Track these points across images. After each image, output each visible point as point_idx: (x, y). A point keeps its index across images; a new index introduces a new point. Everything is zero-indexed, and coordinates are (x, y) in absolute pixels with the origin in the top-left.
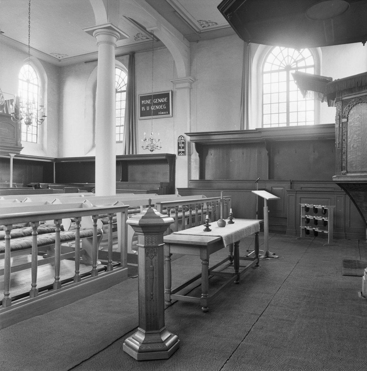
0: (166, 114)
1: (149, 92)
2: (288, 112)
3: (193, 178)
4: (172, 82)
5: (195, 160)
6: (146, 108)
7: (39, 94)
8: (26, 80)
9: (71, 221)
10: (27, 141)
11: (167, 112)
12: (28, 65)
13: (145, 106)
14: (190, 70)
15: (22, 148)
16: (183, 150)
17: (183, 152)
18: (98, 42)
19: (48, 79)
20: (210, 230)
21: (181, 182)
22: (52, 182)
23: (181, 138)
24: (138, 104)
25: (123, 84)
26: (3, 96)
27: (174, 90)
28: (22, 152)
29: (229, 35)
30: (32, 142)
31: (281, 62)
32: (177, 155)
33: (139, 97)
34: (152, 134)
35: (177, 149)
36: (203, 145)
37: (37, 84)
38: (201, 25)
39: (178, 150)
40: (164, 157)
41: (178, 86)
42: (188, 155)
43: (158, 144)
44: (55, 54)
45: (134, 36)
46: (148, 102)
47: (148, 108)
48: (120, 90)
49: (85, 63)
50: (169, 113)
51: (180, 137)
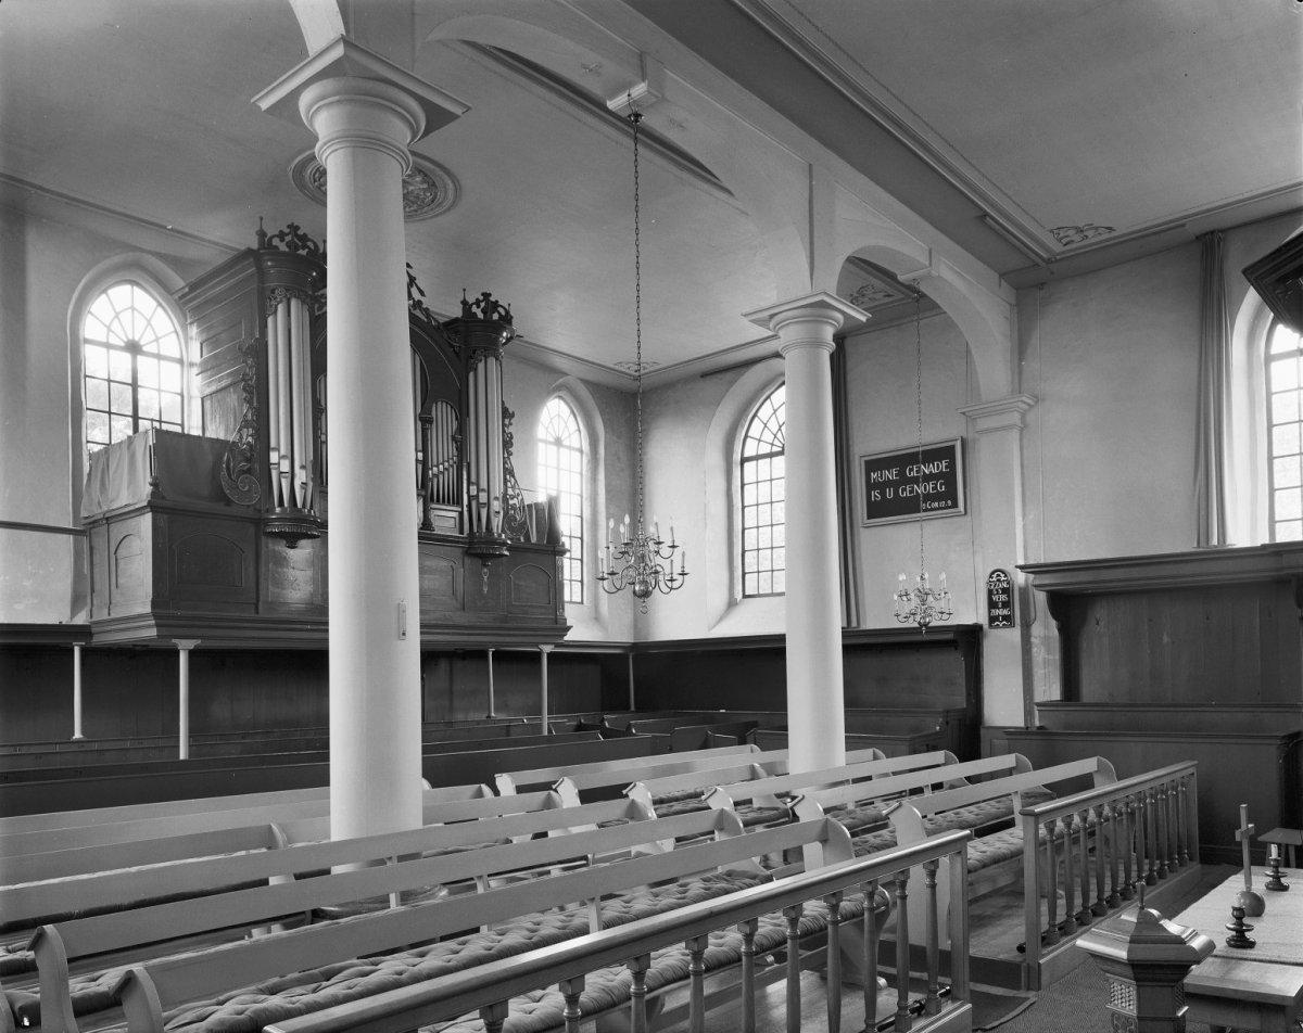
0: (947, 507)
1: (892, 448)
3: (1039, 697)
4: (964, 413)
5: (1046, 639)
6: (883, 494)
8: (123, 344)
11: (949, 502)
13: (882, 486)
14: (1020, 373)
15: (569, 628)
16: (1005, 612)
17: (1005, 618)
19: (606, 432)
20: (1251, 945)
21: (1003, 706)
23: (999, 575)
24: (858, 484)
27: (970, 436)
28: (570, 637)
32: (986, 627)
33: (863, 464)
34: (926, 576)
35: (987, 610)
36: (1073, 599)
38: (1060, 240)
39: (990, 612)
40: (950, 636)
41: (983, 424)
42: (1022, 626)
43: (942, 605)
46: (891, 475)
47: (890, 493)
49: (702, 376)
50: (955, 505)
51: (993, 573)
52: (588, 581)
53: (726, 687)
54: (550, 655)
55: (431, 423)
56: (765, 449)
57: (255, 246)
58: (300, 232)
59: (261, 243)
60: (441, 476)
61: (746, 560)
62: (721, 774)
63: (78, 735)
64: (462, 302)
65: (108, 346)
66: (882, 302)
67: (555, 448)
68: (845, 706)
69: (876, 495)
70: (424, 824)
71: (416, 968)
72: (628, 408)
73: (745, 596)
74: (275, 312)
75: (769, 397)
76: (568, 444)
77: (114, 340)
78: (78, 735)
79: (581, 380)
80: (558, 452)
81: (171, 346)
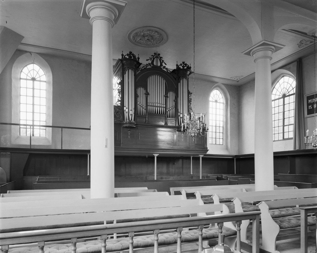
2: (283, 133)
7: (224, 109)
15: (208, 150)
18: (255, 59)
22: (232, 173)
25: (291, 88)
28: (208, 153)
29: (19, 50)
31: (27, 75)
45: (298, 44)
48: (288, 94)
52: (225, 138)
53: (239, 167)
54: (202, 158)
55: (168, 97)
56: (277, 97)
57: (121, 58)
58: (185, 63)
60: (170, 111)
63: (192, 173)
64: (122, 55)
65: (27, 79)
66: (309, 45)
67: (215, 103)
69: (310, 107)
71: (184, 236)
72: (238, 91)
74: (180, 82)
75: (278, 81)
77: (28, 78)
81: (44, 78)
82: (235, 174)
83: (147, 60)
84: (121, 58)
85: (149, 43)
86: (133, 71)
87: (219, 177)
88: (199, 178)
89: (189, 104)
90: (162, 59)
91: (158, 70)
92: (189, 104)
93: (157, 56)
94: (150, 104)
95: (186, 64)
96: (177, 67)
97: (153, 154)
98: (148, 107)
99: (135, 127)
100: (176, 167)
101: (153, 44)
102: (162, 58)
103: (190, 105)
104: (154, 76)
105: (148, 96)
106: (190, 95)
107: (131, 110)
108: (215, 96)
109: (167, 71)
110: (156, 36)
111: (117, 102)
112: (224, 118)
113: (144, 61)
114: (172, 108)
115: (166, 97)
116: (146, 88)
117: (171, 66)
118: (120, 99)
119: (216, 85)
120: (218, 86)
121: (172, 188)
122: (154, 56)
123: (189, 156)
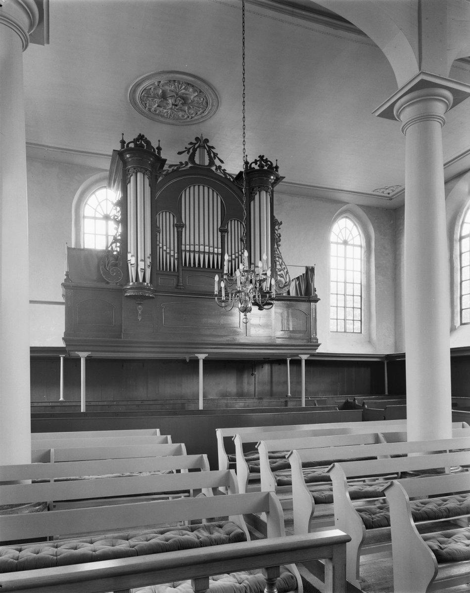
8: (342, 242)
9: (314, 501)
10: (345, 332)
12: (345, 219)
15: (318, 345)
26: (287, 271)
28: (320, 350)
30: (337, 332)
37: (360, 244)
44: (380, 189)
53: (377, 383)
54: (306, 361)
58: (264, 158)
59: (123, 147)
60: (233, 261)
61: (463, 302)
62: (344, 440)
63: (61, 399)
65: (95, 218)
67: (343, 246)
68: (452, 395)
70: (453, 437)
73: (462, 324)
74: (254, 199)
76: (352, 243)
77: (98, 215)
78: (61, 399)
79: (358, 205)
80: (107, 225)
82: (386, 395)
83: (180, 153)
84: (118, 147)
85: (180, 114)
86: (146, 177)
87: (349, 402)
88: (301, 405)
89: (276, 246)
90: (213, 150)
91: (201, 170)
92: (276, 246)
93: (202, 144)
94: (188, 247)
95: (267, 159)
96: (247, 167)
97: (196, 355)
98: (183, 253)
99: (152, 298)
100: (256, 380)
101: (188, 117)
102: (213, 148)
103: (278, 248)
104: (196, 187)
105: (184, 229)
106: (277, 227)
107: (141, 260)
108: (343, 231)
109: (226, 177)
110: (192, 96)
111: (112, 243)
112: (364, 276)
113: (172, 157)
114: (237, 255)
115: (223, 231)
116: (178, 213)
117: (233, 166)
118: (119, 238)
119: (345, 207)
120: (349, 211)
121: (219, 429)
122: (196, 144)
123: (284, 358)
